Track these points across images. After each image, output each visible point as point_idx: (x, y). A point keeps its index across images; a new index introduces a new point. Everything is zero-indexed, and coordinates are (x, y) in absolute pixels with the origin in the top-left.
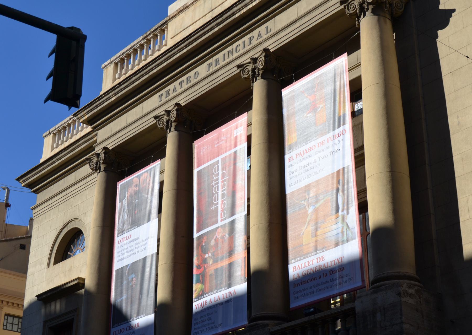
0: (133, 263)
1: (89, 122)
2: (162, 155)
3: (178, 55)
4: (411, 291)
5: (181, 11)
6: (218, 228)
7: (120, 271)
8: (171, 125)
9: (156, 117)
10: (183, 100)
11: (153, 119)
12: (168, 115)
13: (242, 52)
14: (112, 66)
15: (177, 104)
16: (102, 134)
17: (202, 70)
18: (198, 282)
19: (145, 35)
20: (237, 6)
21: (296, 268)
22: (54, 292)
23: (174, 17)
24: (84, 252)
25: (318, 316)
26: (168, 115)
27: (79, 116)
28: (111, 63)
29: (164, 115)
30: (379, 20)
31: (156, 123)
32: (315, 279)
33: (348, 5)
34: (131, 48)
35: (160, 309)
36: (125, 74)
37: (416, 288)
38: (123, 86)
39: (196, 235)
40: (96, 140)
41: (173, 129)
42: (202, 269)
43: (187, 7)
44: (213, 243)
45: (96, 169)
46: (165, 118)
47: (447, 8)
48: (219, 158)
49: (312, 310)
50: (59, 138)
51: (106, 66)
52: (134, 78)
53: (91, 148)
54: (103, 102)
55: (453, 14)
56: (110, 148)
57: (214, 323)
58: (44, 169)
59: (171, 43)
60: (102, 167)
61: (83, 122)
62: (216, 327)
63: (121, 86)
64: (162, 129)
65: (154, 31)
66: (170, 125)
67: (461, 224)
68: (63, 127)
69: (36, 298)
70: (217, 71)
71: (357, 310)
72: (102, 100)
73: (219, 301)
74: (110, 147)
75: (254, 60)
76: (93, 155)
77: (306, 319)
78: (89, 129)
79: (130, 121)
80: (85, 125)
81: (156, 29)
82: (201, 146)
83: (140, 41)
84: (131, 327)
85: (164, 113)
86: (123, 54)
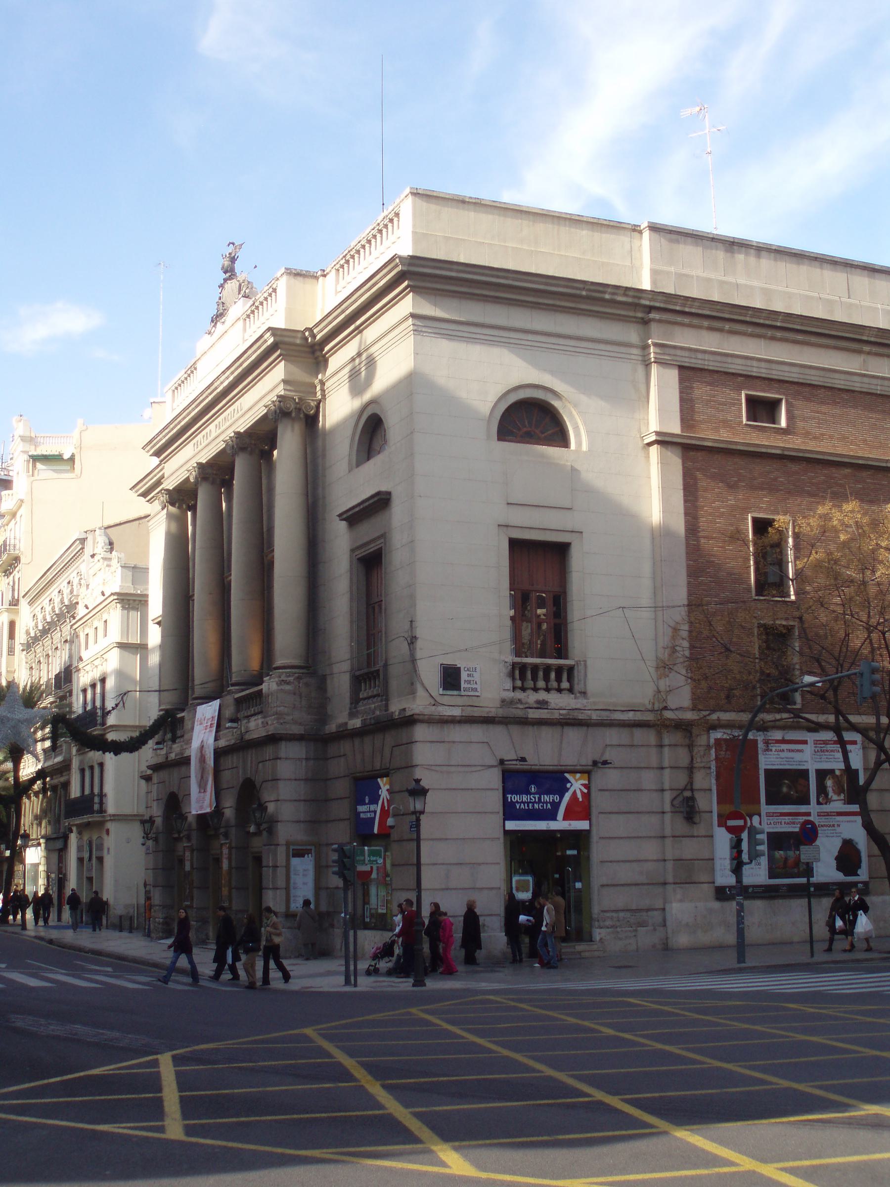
1: (157, 454)
4: (291, 679)
13: (240, 413)
17: (212, 430)
78: (156, 461)
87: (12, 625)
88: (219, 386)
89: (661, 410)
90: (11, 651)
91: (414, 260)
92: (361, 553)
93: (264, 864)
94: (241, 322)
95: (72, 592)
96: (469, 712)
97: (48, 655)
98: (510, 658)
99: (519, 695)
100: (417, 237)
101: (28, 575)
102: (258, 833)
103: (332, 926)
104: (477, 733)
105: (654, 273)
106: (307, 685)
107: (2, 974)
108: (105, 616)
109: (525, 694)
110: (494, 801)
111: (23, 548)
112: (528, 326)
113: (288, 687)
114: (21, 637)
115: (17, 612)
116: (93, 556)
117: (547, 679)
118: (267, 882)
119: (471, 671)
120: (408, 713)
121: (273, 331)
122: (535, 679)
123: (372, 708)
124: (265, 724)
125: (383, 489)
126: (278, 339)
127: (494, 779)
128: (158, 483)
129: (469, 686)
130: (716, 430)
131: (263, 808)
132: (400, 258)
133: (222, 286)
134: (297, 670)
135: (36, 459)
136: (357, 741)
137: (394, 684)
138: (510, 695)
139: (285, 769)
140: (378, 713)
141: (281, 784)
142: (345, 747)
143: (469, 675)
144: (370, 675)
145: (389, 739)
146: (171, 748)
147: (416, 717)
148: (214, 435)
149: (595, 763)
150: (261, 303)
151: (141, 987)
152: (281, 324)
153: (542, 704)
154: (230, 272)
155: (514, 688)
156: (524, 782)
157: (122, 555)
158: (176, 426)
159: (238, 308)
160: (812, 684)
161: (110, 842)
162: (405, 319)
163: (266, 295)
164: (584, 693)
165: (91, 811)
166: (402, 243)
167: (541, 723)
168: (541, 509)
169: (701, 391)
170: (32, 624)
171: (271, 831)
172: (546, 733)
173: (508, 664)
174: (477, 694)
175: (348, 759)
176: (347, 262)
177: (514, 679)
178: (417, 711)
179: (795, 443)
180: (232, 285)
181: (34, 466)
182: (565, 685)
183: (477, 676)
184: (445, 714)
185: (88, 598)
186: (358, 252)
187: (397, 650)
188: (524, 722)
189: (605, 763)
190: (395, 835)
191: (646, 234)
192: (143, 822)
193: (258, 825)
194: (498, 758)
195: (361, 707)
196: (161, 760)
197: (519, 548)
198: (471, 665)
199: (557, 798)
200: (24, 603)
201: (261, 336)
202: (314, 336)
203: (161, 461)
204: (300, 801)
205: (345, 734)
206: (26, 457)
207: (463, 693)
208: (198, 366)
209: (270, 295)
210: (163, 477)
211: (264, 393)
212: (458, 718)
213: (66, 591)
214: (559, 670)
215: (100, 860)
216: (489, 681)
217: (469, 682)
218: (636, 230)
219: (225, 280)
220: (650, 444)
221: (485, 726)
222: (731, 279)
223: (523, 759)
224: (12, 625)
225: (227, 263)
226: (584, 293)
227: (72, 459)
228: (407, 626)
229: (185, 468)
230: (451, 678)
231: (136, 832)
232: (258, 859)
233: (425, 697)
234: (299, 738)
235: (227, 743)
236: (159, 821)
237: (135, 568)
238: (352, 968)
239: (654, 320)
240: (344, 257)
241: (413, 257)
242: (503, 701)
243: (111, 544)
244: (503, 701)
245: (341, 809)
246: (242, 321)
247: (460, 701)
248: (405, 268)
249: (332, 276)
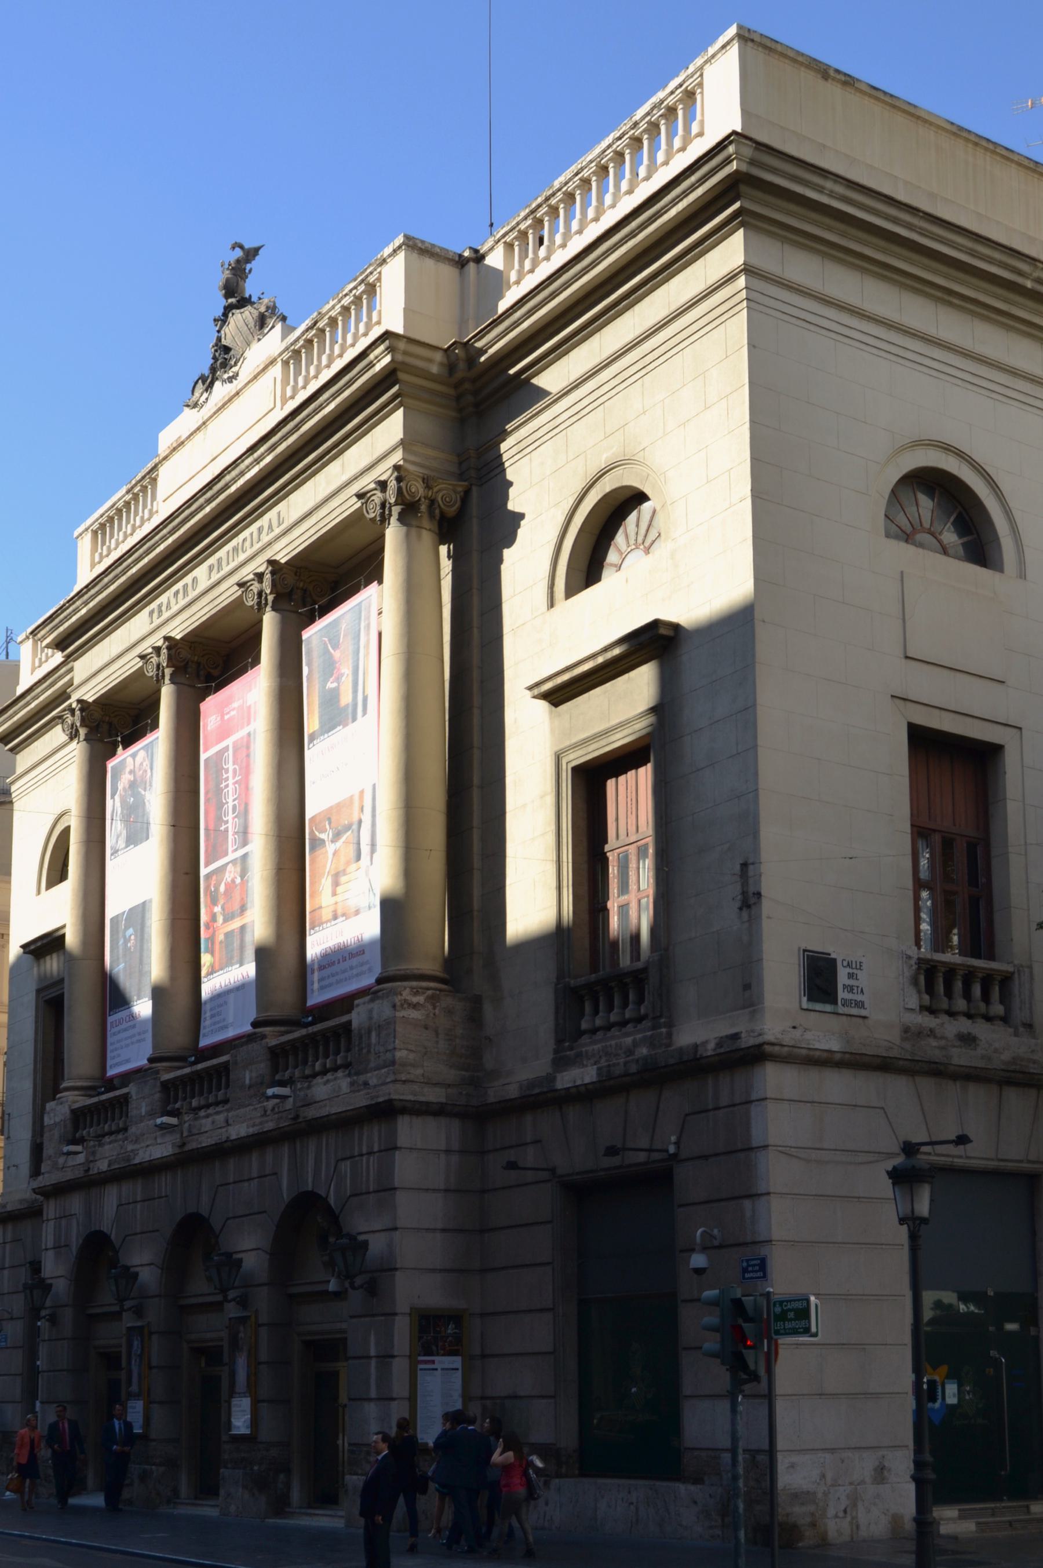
0: (130, 910)
1: (60, 644)
2: (376, 575)
3: (162, 547)
4: (420, 999)
5: (174, 449)
6: (228, 864)
7: (115, 920)
8: (390, 511)
9: (360, 496)
10: (178, 630)
11: (355, 499)
12: (159, 655)
13: (277, 531)
14: (88, 536)
15: (271, 562)
16: (82, 667)
17: (201, 575)
18: (206, 951)
19: (129, 486)
20: (229, 472)
21: (316, 945)
22: (39, 944)
23: (165, 458)
24: (661, 550)
25: (200, 1066)
26: (159, 655)
27: (39, 636)
28: (87, 530)
29: (375, 489)
30: (408, 535)
31: (241, 596)
32: (333, 963)
33: (366, 503)
34: (112, 506)
35: (158, 994)
36: (365, 334)
37: (430, 992)
38: (93, 592)
39: (203, 871)
40: (72, 679)
41: (167, 680)
42: (211, 930)
43: (183, 443)
44: (222, 888)
45: (73, 736)
46: (255, 587)
47: (517, 510)
48: (229, 742)
49: (310, 1019)
50: (524, 255)
51: (81, 535)
52: (106, 580)
53: (63, 696)
54: (129, 568)
55: (522, 523)
56: (283, 561)
57: (224, 1020)
58: (16, 713)
59: (164, 510)
60: (82, 732)
61: (48, 646)
62: (226, 1027)
63: (89, 590)
64: (373, 520)
65: (140, 480)
66: (387, 512)
67: (507, 888)
68: (650, 123)
69: (22, 950)
70: (218, 583)
71: (355, 1025)
72: (68, 611)
73: (230, 987)
74: (283, 558)
75: (383, 485)
76: (64, 710)
77: (303, 1032)
78: (58, 657)
79: (115, 652)
80: (50, 650)
81: (143, 478)
82: (213, 711)
83: (124, 496)
84: (132, 1017)
85: (251, 576)
86: (101, 516)
88: (234, 480)
94: (277, 370)
106: (449, 1012)
109: (938, 1021)
126: (399, 357)
128: (63, 696)
129: (850, 996)
134: (432, 984)
140: (644, 1051)
143: (851, 976)
146: (94, 1153)
147: (768, 1049)
150: (333, 322)
153: (968, 1040)
158: (117, 577)
163: (346, 301)
164: (1029, 1026)
168: (958, 674)
171: (372, 1289)
173: (913, 962)
174: (863, 1012)
178: (769, 1037)
184: (817, 1046)
194: (902, 1139)
197: (924, 743)
203: (68, 657)
204: (434, 1230)
205: (541, 1099)
207: (841, 1009)
209: (358, 300)
210: (70, 683)
211: (345, 478)
212: (838, 1056)
214: (987, 980)
217: (850, 989)
219: (228, 310)
226: (1029, 284)
229: (138, 650)
230: (820, 978)
233: (782, 1008)
235: (251, 1131)
240: (533, 212)
242: (906, 1030)
244: (906, 1030)
246: (279, 364)
248: (744, 168)
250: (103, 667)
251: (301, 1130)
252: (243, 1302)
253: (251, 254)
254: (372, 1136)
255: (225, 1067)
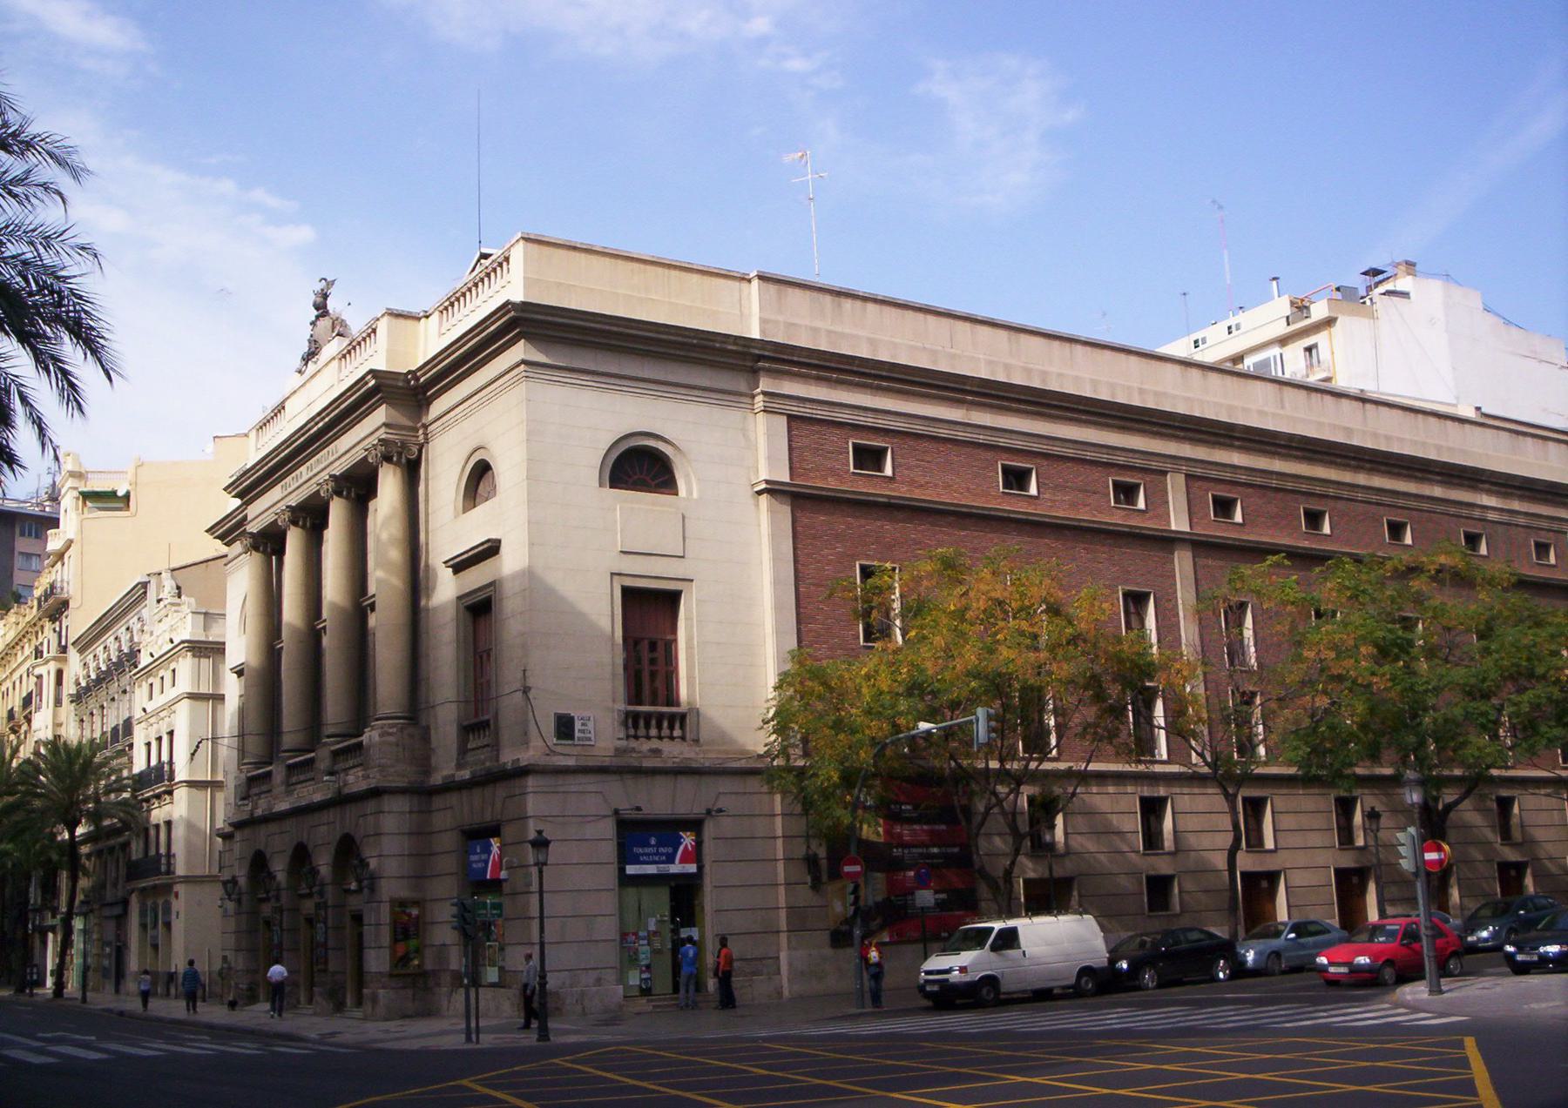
1: (239, 495)
10: (337, 470)
16: (253, 510)
17: (304, 472)
78: (238, 502)
87: (60, 673)
89: (770, 458)
90: (58, 702)
91: (525, 306)
92: (470, 601)
93: (366, 921)
95: (131, 639)
96: (583, 762)
97: (102, 707)
98: (621, 706)
99: (633, 744)
100: (528, 283)
101: (78, 622)
102: (360, 890)
103: (438, 985)
104: (590, 783)
105: (763, 321)
106: (411, 736)
107: (6, 1052)
108: (173, 666)
110: (609, 850)
111: (72, 590)
112: (640, 375)
113: (392, 739)
114: (69, 688)
115: (65, 660)
116: (159, 601)
117: (659, 727)
118: (368, 938)
119: (585, 721)
120: (523, 764)
121: (373, 373)
122: (647, 726)
123: (481, 761)
124: (366, 777)
125: (493, 537)
127: (608, 829)
130: (824, 478)
131: (364, 864)
132: (514, 304)
133: (313, 323)
135: (87, 496)
136: (465, 793)
137: (506, 736)
138: (624, 743)
139: (389, 823)
141: (385, 840)
142: (453, 799)
144: (478, 725)
145: (501, 791)
148: (305, 478)
149: (709, 812)
151: (105, 1056)
152: (381, 366)
153: (656, 752)
154: (321, 308)
155: (628, 737)
156: (635, 833)
157: (192, 600)
159: (332, 348)
160: (928, 732)
161: (178, 905)
162: (518, 365)
164: (696, 741)
165: (158, 872)
166: (512, 288)
167: (654, 772)
169: (807, 436)
170: (82, 673)
171: (372, 889)
172: (661, 783)
175: (450, 815)
176: (452, 304)
177: (627, 728)
179: (902, 491)
180: (325, 323)
181: (84, 503)
182: (677, 732)
183: (590, 725)
185: (152, 645)
186: (464, 295)
187: (509, 704)
188: (638, 772)
189: (720, 811)
190: (506, 888)
191: (755, 282)
192: (225, 883)
193: (359, 881)
195: (470, 758)
196: (245, 817)
198: (586, 714)
199: (670, 850)
200: (73, 653)
201: (363, 378)
202: (417, 379)
205: (450, 787)
206: (75, 494)
208: (287, 405)
213: (125, 638)
215: (168, 925)
216: (602, 730)
218: (745, 279)
219: (317, 317)
220: (759, 493)
221: (599, 777)
222: (838, 329)
223: (638, 809)
224: (60, 673)
225: (319, 300)
227: (127, 496)
228: (520, 675)
230: (565, 727)
231: (213, 895)
232: (358, 919)
234: (402, 791)
236: (242, 881)
237: (206, 614)
238: (473, 1025)
239: (764, 369)
241: (524, 303)
242: (617, 749)
243: (178, 588)
244: (617, 749)
245: (448, 863)
247: (575, 751)
249: (435, 317)
250: (266, 509)
251: (342, 800)
252: (321, 894)
253: (331, 284)
254: (371, 806)
255: (312, 760)
